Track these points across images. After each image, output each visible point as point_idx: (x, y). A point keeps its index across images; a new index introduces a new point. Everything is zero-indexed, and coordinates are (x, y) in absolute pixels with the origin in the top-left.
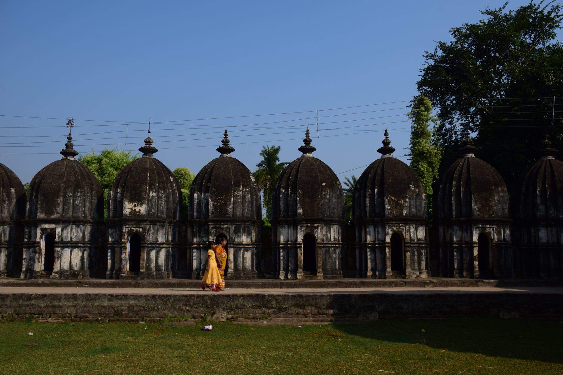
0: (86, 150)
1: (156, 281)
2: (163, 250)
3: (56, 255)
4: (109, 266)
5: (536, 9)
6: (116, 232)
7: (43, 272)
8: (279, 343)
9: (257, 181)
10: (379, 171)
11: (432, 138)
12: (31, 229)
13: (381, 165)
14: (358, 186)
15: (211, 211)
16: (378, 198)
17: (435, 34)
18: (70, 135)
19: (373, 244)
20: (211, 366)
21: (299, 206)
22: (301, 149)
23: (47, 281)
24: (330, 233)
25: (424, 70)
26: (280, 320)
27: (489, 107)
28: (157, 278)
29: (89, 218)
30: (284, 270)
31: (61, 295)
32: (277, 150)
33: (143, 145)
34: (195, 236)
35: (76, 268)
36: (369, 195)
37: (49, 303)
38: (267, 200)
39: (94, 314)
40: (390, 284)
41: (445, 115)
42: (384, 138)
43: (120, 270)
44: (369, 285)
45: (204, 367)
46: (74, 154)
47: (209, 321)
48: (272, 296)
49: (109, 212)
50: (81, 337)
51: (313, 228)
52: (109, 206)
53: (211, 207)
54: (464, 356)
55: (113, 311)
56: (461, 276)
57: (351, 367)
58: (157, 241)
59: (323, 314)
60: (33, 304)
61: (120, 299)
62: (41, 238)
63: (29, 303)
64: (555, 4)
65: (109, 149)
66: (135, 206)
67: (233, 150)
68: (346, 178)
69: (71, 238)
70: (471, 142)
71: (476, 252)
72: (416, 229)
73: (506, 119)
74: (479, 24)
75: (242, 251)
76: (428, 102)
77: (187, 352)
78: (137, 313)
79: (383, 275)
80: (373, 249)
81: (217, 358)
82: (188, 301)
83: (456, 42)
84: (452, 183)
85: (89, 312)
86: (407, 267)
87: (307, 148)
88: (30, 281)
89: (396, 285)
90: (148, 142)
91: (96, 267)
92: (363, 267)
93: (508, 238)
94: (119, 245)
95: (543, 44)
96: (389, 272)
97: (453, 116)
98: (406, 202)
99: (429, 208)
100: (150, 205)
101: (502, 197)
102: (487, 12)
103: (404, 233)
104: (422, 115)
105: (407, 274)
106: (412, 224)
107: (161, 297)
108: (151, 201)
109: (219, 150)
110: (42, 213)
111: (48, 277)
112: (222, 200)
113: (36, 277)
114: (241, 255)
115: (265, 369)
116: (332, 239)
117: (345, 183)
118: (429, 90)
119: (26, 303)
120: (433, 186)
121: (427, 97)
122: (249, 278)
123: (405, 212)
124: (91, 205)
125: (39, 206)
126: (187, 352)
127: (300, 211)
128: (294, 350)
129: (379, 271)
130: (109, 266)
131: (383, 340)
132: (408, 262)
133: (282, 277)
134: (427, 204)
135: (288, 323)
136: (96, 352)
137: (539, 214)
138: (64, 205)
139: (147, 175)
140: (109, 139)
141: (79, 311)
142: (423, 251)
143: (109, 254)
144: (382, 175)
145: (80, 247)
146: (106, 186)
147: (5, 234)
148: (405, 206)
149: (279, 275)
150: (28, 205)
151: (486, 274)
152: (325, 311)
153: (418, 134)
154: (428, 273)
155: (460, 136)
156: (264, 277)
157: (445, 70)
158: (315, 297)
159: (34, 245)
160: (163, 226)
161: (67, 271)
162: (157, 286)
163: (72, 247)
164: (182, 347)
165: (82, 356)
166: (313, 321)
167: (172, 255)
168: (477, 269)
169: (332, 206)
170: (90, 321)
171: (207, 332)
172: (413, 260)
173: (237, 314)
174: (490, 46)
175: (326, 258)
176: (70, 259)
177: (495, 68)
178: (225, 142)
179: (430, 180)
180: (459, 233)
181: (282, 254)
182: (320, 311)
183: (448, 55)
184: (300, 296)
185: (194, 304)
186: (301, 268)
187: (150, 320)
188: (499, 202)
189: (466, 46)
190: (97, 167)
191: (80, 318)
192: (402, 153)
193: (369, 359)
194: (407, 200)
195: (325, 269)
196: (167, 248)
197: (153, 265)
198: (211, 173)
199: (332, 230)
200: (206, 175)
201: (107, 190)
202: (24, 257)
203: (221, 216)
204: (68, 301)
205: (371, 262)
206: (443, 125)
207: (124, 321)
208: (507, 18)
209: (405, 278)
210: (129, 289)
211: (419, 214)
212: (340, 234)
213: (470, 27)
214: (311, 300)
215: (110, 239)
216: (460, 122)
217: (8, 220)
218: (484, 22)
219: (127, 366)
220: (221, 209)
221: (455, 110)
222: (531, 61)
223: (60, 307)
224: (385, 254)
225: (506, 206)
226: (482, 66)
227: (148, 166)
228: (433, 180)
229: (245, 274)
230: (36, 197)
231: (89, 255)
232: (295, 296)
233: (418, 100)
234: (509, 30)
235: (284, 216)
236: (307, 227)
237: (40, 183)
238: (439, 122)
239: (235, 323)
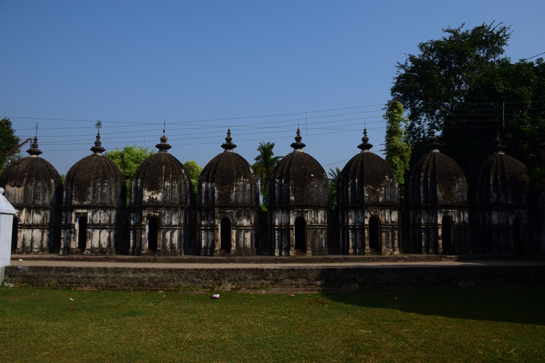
0: (112, 147)
1: (171, 257)
2: (177, 231)
3: (88, 235)
4: (131, 245)
5: (488, 29)
6: (137, 216)
7: (78, 249)
8: (276, 308)
9: (255, 172)
10: (359, 164)
11: (404, 136)
12: (67, 213)
13: (361, 159)
14: (342, 177)
15: (216, 198)
16: (358, 187)
17: (389, 77)
18: (98, 134)
19: (354, 226)
20: (220, 327)
22: (293, 145)
23: (81, 257)
24: (318, 217)
25: (396, 78)
26: (276, 290)
27: (451, 110)
28: (172, 255)
29: (115, 204)
30: (278, 248)
31: (94, 268)
32: (272, 146)
33: (159, 142)
34: (203, 220)
35: (104, 246)
36: (351, 184)
37: (85, 275)
38: (263, 188)
39: (121, 284)
40: (368, 260)
41: (414, 117)
42: (363, 136)
43: (141, 248)
44: (351, 260)
45: (214, 328)
46: (102, 150)
47: (217, 291)
49: (131, 199)
50: (112, 303)
51: (303, 213)
52: (131, 193)
53: (216, 195)
54: (428, 318)
55: (137, 282)
56: (428, 252)
57: (336, 328)
58: (171, 223)
59: (312, 285)
60: (72, 276)
61: (142, 272)
62: (76, 221)
63: (69, 274)
64: (502, 26)
65: (130, 146)
66: (153, 194)
67: (235, 146)
68: (331, 170)
69: (100, 221)
70: (436, 140)
71: (440, 232)
72: (390, 213)
73: (465, 121)
74: (442, 40)
75: (243, 232)
76: (400, 105)
77: (199, 315)
78: (156, 284)
79: (362, 252)
80: (354, 230)
81: (225, 321)
82: (199, 274)
83: (423, 55)
84: (420, 174)
85: (117, 282)
86: (383, 245)
87: (298, 144)
88: (68, 257)
89: (374, 260)
90: (163, 140)
91: (121, 246)
92: (346, 245)
93: (466, 221)
94: (139, 227)
95: (494, 58)
96: (367, 250)
97: (421, 117)
98: (382, 190)
99: (401, 195)
100: (165, 193)
101: (462, 186)
102: (448, 31)
103: (380, 217)
104: (395, 117)
105: (383, 251)
106: (387, 209)
107: (176, 270)
108: (166, 190)
109: (223, 146)
110: (76, 200)
111: (82, 254)
113: (72, 253)
114: (242, 236)
115: (264, 330)
116: (320, 222)
117: (330, 174)
118: (401, 95)
119: (66, 274)
120: (404, 176)
121: (399, 101)
122: (249, 255)
124: (116, 193)
125: (74, 194)
126: (199, 315)
127: (292, 198)
128: (288, 314)
130: (131, 245)
131: (363, 306)
132: (384, 241)
133: (277, 254)
134: (399, 191)
135: (283, 293)
136: (125, 315)
137: (492, 200)
138: (94, 193)
140: (131, 137)
141: (109, 282)
142: (396, 232)
143: (131, 234)
144: (362, 167)
145: (107, 228)
146: (128, 177)
147: (47, 218)
149: (274, 252)
150: (64, 193)
151: (448, 251)
152: (314, 283)
153: (392, 133)
154: (400, 250)
155: (427, 134)
156: (262, 254)
157: (414, 78)
158: (305, 270)
159: (71, 226)
160: (176, 211)
161: (97, 249)
162: (171, 261)
163: (100, 228)
164: (195, 312)
165: (113, 318)
167: (184, 235)
168: (441, 247)
169: (319, 194)
170: (118, 290)
171: (215, 300)
172: (387, 239)
173: (240, 285)
174: (451, 58)
175: (314, 238)
177: (455, 77)
179: (402, 172)
180: (426, 216)
181: (276, 234)
182: (310, 283)
183: (416, 66)
184: (293, 270)
185: (204, 277)
186: (293, 246)
187: (168, 290)
188: (460, 190)
189: (431, 58)
190: (120, 161)
191: (110, 288)
192: (379, 149)
193: (351, 321)
194: (383, 188)
195: (313, 248)
196: (180, 229)
197: (168, 244)
198: (217, 166)
199: (319, 215)
200: (213, 168)
201: (128, 180)
202: (62, 236)
203: (226, 203)
204: (100, 273)
205: (352, 241)
206: (413, 125)
207: (146, 290)
208: (464, 36)
209: (380, 254)
211: (392, 200)
212: (326, 218)
213: (435, 43)
214: (302, 273)
215: (132, 222)
216: (427, 122)
217: (49, 206)
218: (445, 39)
219: (151, 327)
220: (225, 197)
221: (422, 112)
222: (485, 72)
223: (94, 278)
224: (364, 234)
225: (465, 194)
226: (445, 75)
227: (163, 160)
228: (405, 172)
229: (245, 252)
230: (71, 187)
231: (115, 235)
232: (288, 270)
233: (392, 104)
234: (466, 46)
235: (278, 203)
236: (298, 211)
237: (74, 175)
238: (409, 123)
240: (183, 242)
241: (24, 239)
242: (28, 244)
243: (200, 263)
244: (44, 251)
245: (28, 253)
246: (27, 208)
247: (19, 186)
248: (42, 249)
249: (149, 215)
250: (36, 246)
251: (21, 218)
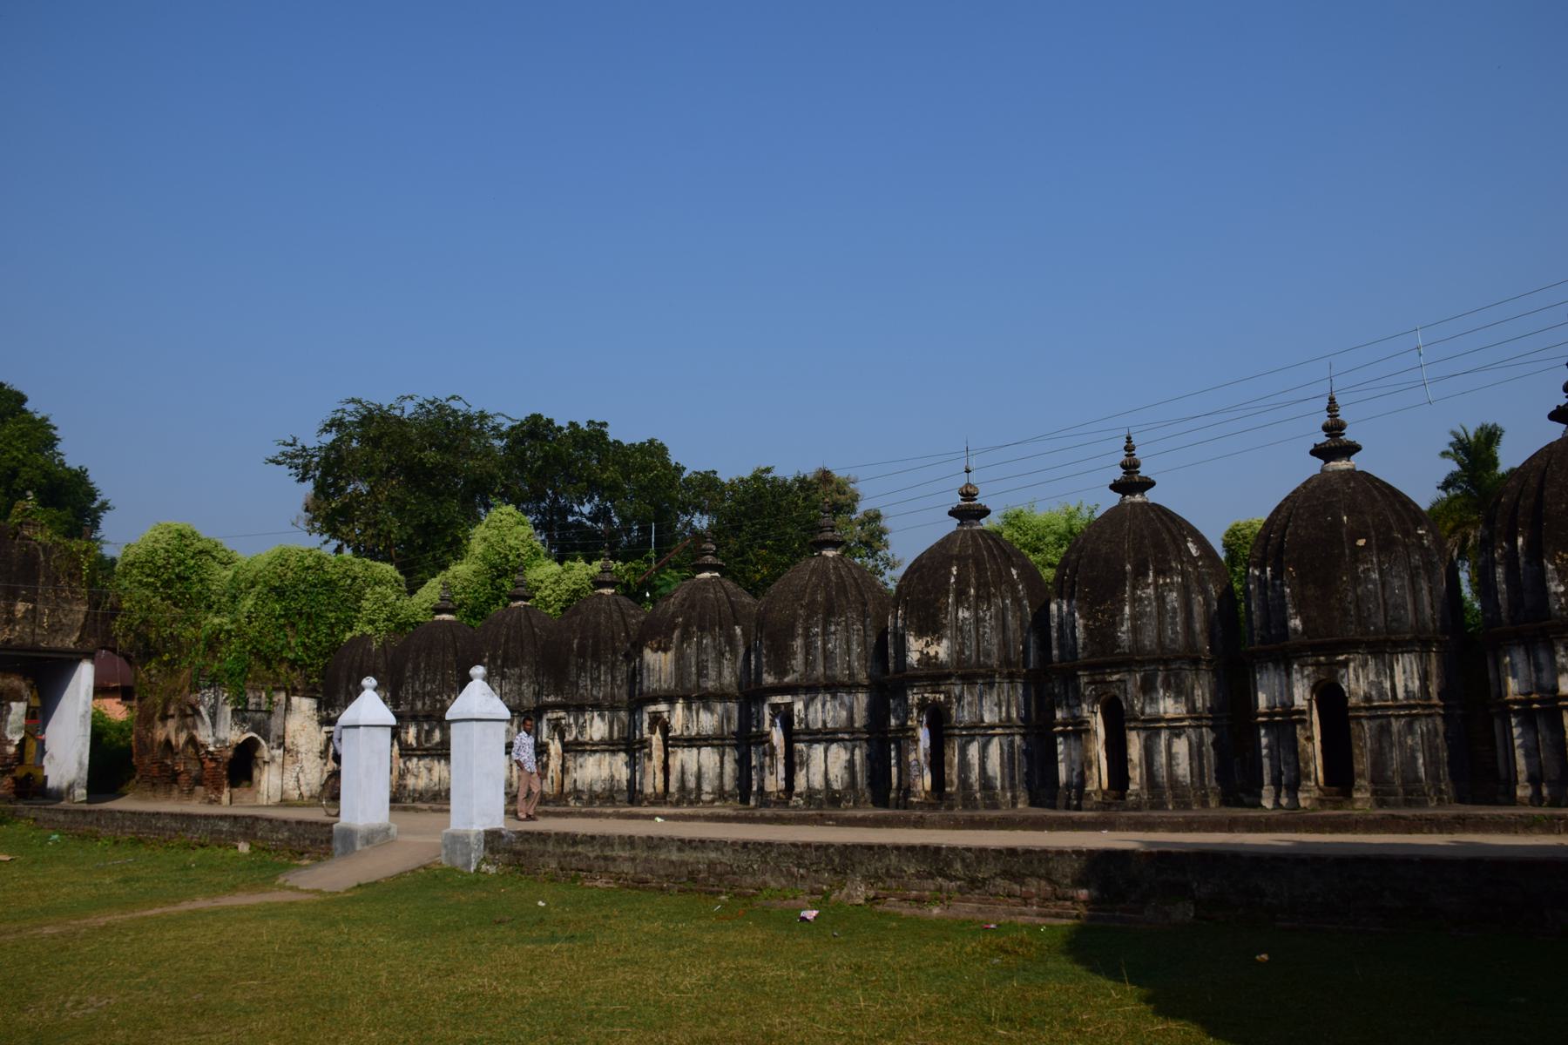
2: (996, 741)
15: (1080, 642)
16: (1528, 562)
21: (1291, 611)
22: (1318, 452)
26: (966, 909)
35: (837, 786)
36: (1503, 556)
48: (952, 849)
58: (982, 721)
59: (1066, 899)
62: (773, 724)
66: (927, 645)
67: (1150, 484)
69: (824, 723)
78: (720, 877)
80: (1528, 718)
85: (651, 871)
90: (968, 495)
91: (879, 787)
108: (960, 629)
112: (1103, 612)
127: (1296, 623)
129: (1550, 784)
133: (1267, 803)
138: (807, 653)
145: (843, 740)
149: (1260, 796)
152: (1070, 893)
156: (1041, 805)
158: (1044, 855)
160: (991, 685)
161: (819, 792)
162: (957, 824)
163: (826, 741)
166: (1039, 915)
171: (805, 925)
175: (1381, 747)
176: (827, 765)
178: (1130, 467)
181: (1264, 741)
182: (1059, 891)
186: (1361, 775)
197: (975, 775)
199: (1398, 669)
205: (1527, 756)
210: (1020, 832)
215: (893, 722)
217: (734, 690)
220: (1102, 635)
223: (614, 859)
236: (1318, 664)
240: (1500, 752)
241: (683, 772)
242: (691, 783)
243: (1024, 829)
244: (726, 800)
245: (691, 803)
246: (684, 698)
247: (665, 650)
248: (721, 794)
249: (924, 699)
250: (706, 787)
251: (673, 722)
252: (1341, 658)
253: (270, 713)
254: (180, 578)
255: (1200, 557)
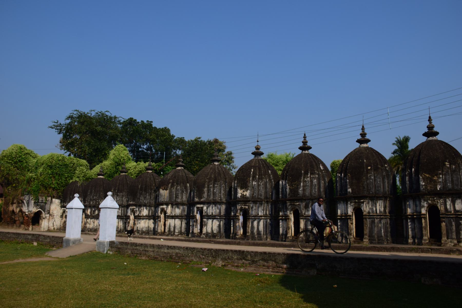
2: (262, 221)
15: (288, 193)
16: (415, 176)
21: (348, 187)
22: (358, 141)
24: (376, 207)
26: (251, 269)
28: (258, 240)
35: (215, 232)
40: (427, 251)
42: (428, 123)
48: (248, 252)
51: (360, 203)
58: (258, 214)
62: (197, 213)
66: (243, 192)
67: (369, 141)
69: (212, 213)
78: (179, 258)
79: (420, 243)
80: (413, 220)
85: (159, 255)
86: (443, 236)
87: (431, 132)
90: (257, 148)
96: (425, 240)
98: (439, 178)
103: (439, 205)
105: (443, 242)
106: (448, 197)
108: (253, 188)
109: (300, 148)
112: (295, 185)
123: (439, 187)
127: (350, 190)
129: (418, 239)
132: (444, 231)
138: (208, 193)
139: (251, 171)
145: (217, 218)
148: (439, 182)
152: (281, 266)
156: (274, 240)
158: (274, 254)
160: (261, 204)
161: (210, 233)
162: (250, 245)
166: (272, 272)
171: (204, 272)
175: (372, 227)
176: (212, 226)
178: (363, 135)
194: (441, 176)
197: (255, 230)
199: (378, 205)
205: (412, 230)
209: (440, 245)
215: (232, 214)
220: (294, 191)
223: (148, 251)
236: (355, 202)
239: (225, 268)
241: (170, 226)
242: (172, 229)
245: (172, 235)
247: (166, 190)
250: (177, 231)
252: (362, 201)
253: (46, 203)
254: (20, 161)
255: (323, 170)
